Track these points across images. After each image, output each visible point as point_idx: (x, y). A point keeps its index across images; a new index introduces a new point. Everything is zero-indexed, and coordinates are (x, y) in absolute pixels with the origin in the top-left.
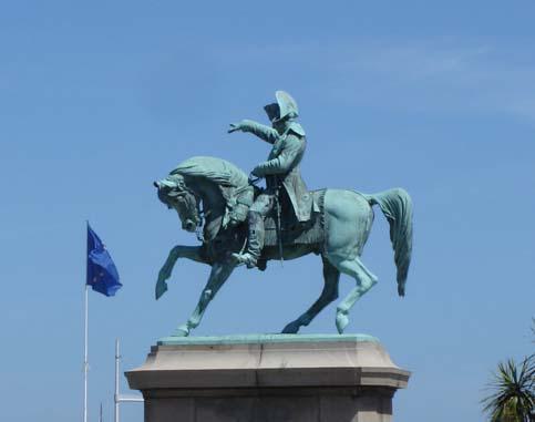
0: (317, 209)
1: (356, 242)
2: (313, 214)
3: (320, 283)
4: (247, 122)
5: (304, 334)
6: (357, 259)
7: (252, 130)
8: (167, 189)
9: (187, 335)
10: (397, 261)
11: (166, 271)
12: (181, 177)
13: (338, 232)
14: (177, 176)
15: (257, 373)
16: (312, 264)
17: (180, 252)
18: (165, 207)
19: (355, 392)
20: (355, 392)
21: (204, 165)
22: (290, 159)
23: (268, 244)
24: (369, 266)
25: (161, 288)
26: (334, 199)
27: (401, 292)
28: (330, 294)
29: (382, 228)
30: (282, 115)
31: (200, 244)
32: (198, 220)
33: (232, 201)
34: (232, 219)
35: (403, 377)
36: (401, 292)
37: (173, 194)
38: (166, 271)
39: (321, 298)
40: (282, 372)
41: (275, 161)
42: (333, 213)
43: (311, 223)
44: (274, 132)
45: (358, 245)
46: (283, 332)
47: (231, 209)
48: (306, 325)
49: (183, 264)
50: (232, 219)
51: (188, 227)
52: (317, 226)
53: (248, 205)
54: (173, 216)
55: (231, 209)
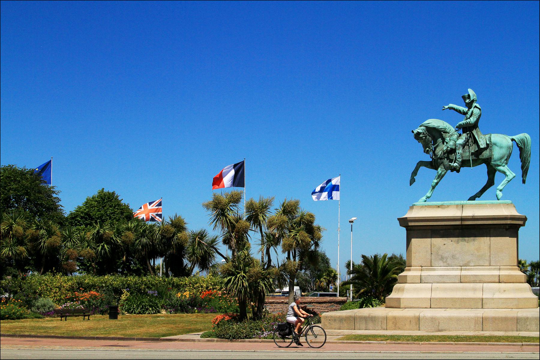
0: (488, 142)
1: (505, 158)
2: (487, 145)
3: (485, 179)
4: (451, 105)
5: (477, 201)
6: (506, 166)
7: (454, 109)
8: (419, 133)
9: (425, 201)
10: (522, 167)
11: (415, 173)
12: (425, 128)
13: (497, 153)
14: (423, 128)
15: (462, 219)
16: (484, 167)
17: (421, 163)
18: (417, 141)
19: (507, 227)
20: (507, 227)
21: (434, 123)
22: (475, 119)
23: (465, 159)
24: (510, 172)
25: (412, 181)
26: (496, 138)
27: (524, 182)
28: (491, 183)
29: (516, 152)
30: (472, 99)
31: (431, 160)
32: (273, 309)
33: (447, 139)
34: (448, 147)
35: (525, 219)
36: (524, 182)
37: (421, 136)
38: (415, 173)
39: (22, 174)
40: (474, 219)
41: (468, 121)
42: (495, 144)
43: (485, 149)
44: (466, 109)
45: (506, 160)
46: (469, 200)
47: (447, 143)
48: (479, 197)
49: (422, 169)
50: (448, 147)
51: (427, 152)
52: (488, 150)
53: (455, 139)
54: (420, 145)
55: (447, 143)
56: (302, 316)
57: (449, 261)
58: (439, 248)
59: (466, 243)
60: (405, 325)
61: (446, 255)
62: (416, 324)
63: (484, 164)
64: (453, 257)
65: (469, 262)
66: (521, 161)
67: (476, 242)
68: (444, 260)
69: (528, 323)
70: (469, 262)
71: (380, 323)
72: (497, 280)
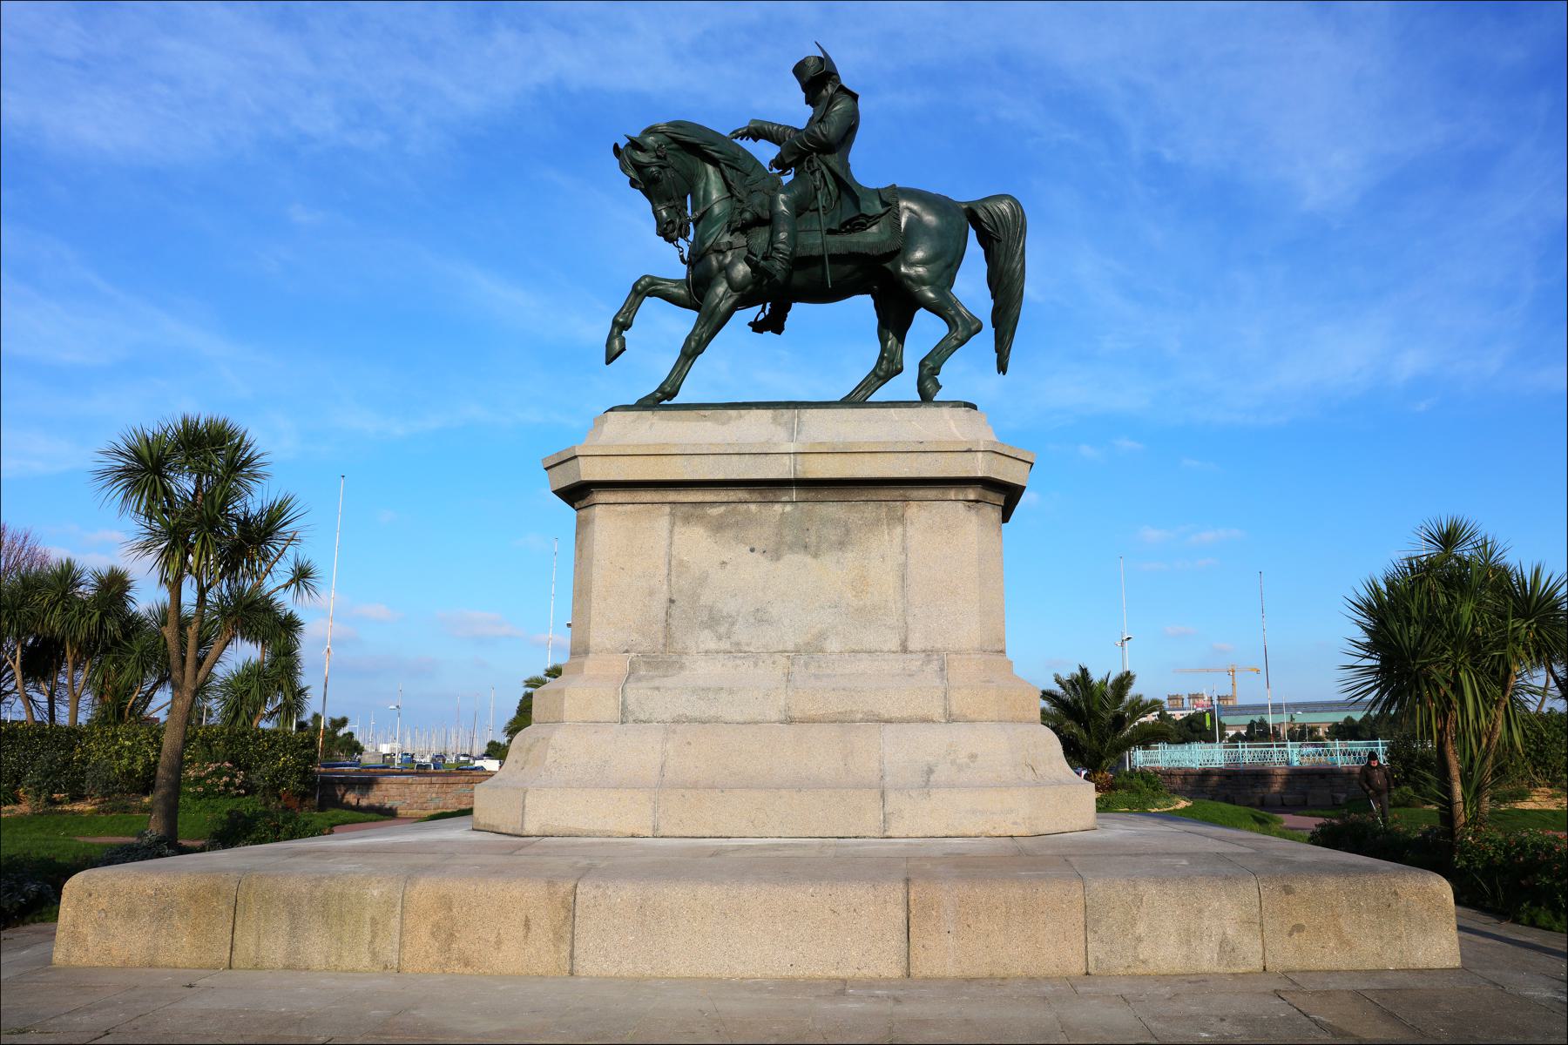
3: (871, 352)
11: (621, 325)
17: (646, 289)
38: (621, 325)
56: (932, 743)
57: (742, 634)
58: (703, 579)
59: (808, 559)
60: (499, 943)
61: (729, 606)
62: (558, 938)
63: (869, 296)
64: (760, 617)
65: (822, 636)
66: (994, 297)
67: (850, 555)
68: (722, 630)
69: (1141, 929)
70: (822, 636)
71: (367, 930)
72: (937, 712)
